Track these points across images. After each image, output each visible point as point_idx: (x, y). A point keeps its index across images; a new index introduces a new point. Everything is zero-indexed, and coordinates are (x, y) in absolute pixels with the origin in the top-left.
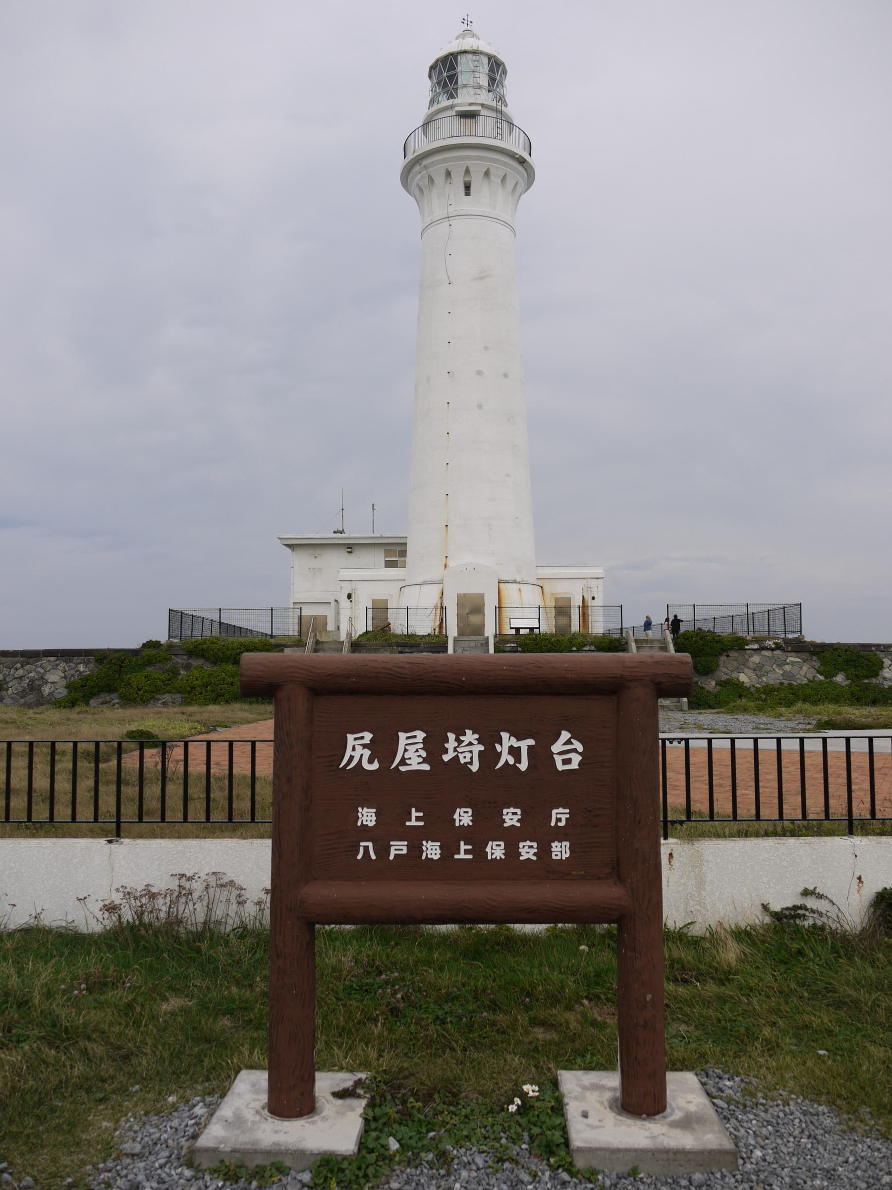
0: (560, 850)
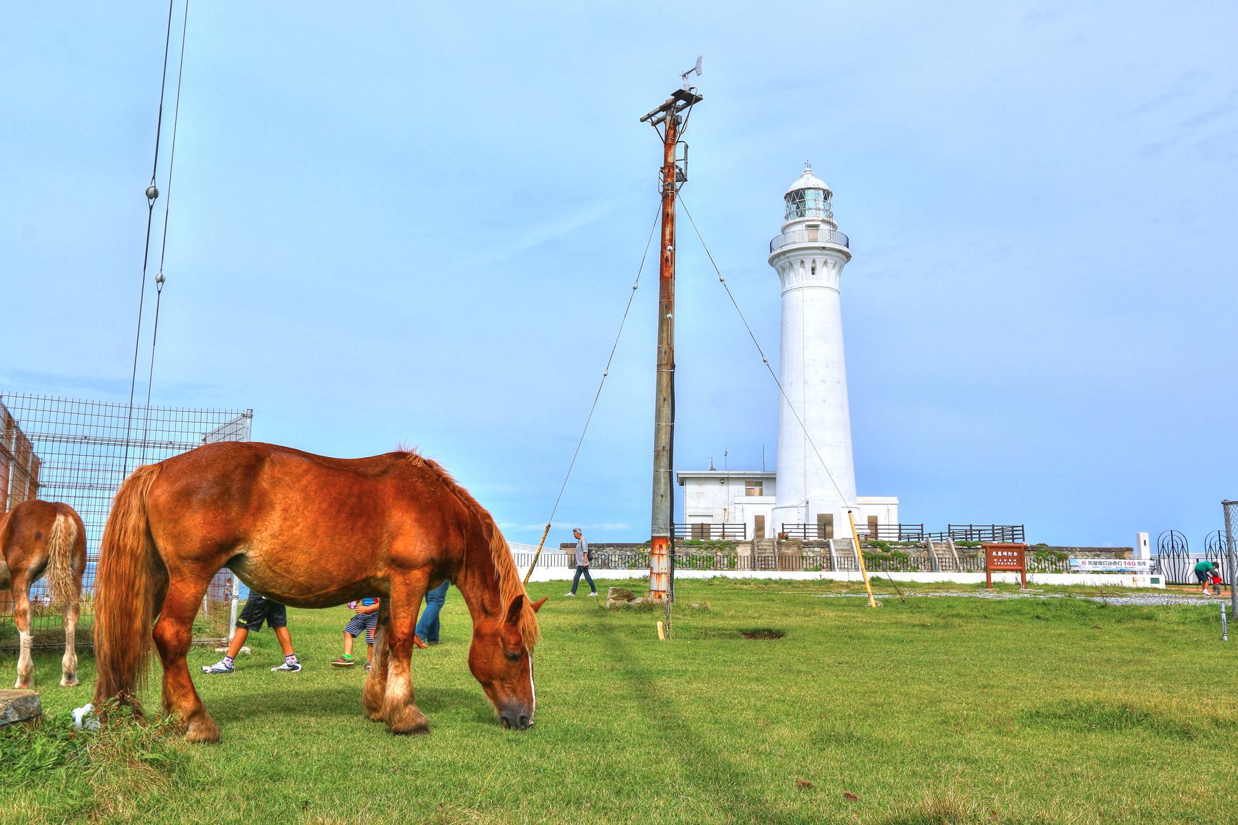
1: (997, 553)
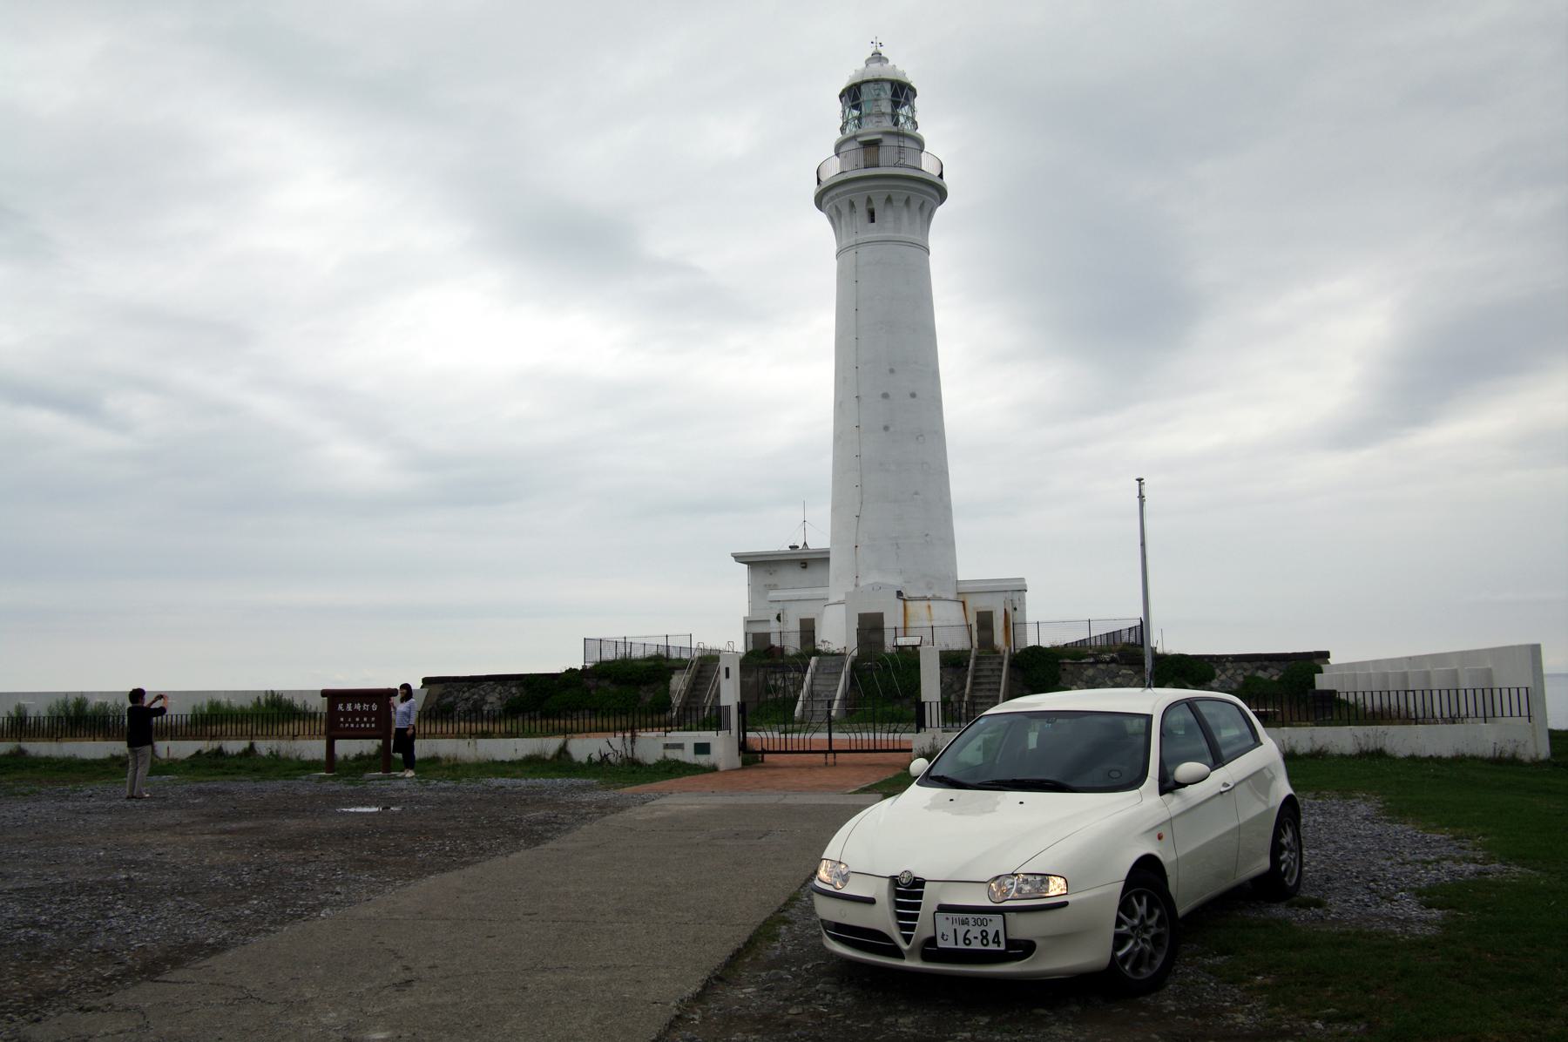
0: (373, 725)
1: (345, 707)
